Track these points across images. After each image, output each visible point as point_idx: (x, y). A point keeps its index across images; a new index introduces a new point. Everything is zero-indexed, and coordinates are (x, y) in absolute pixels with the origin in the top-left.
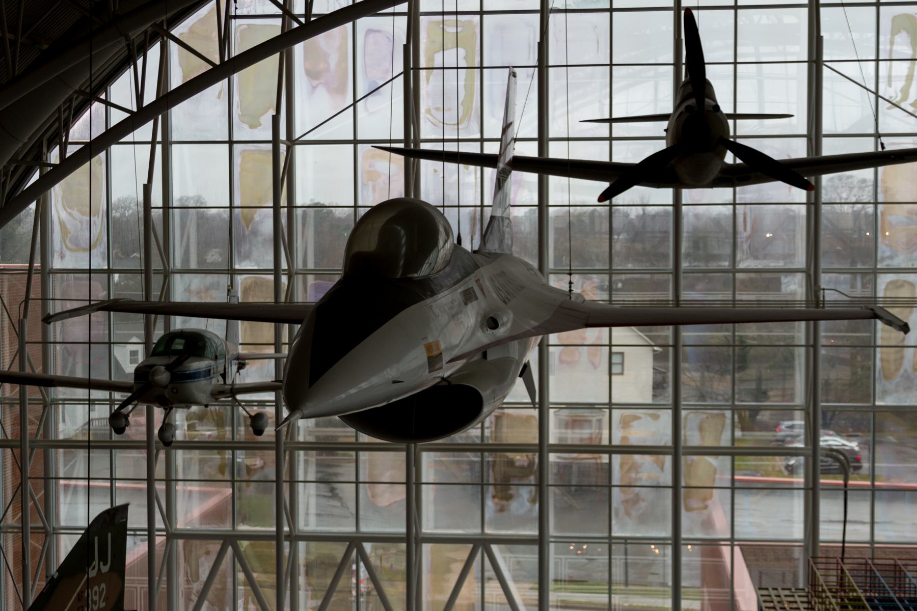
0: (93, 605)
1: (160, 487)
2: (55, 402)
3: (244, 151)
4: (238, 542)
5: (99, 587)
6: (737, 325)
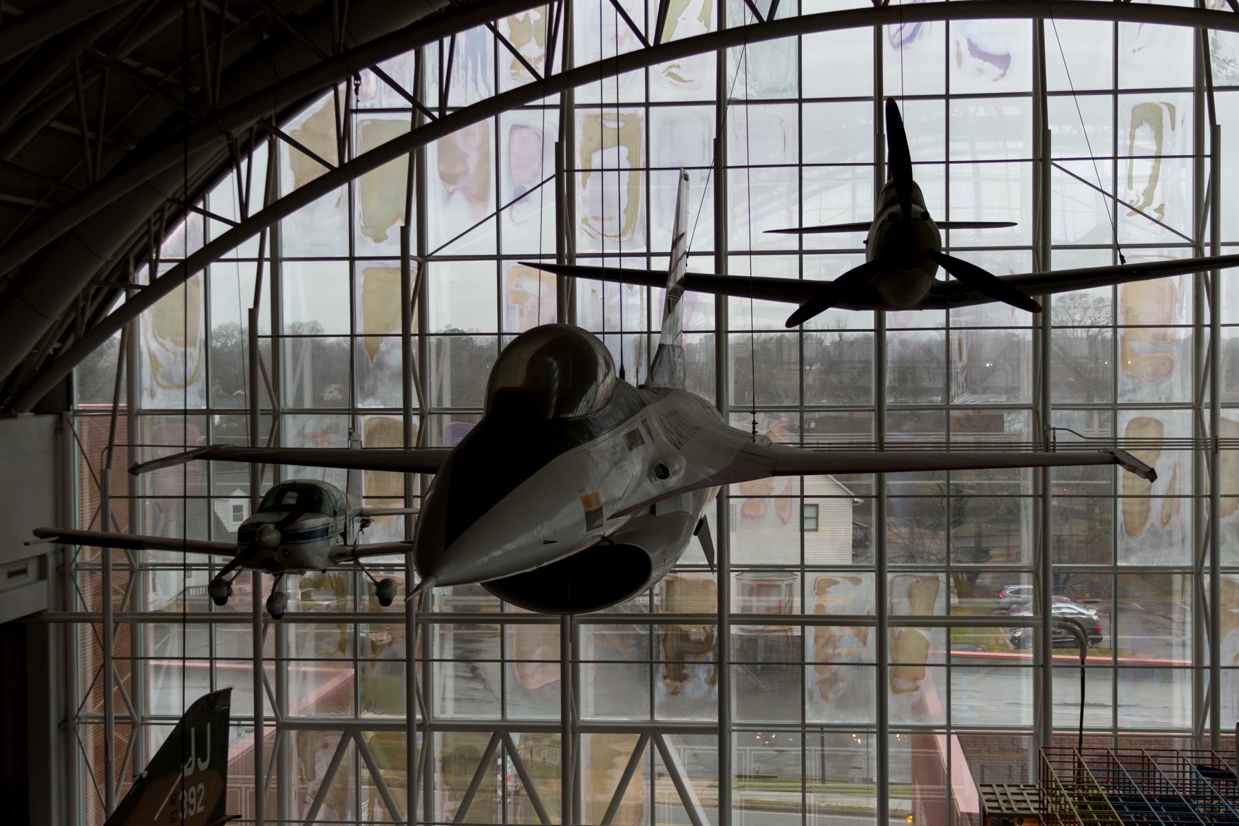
1: (269, 668)
2: (145, 568)
3: (367, 269)
4: (362, 732)
6: (951, 472)
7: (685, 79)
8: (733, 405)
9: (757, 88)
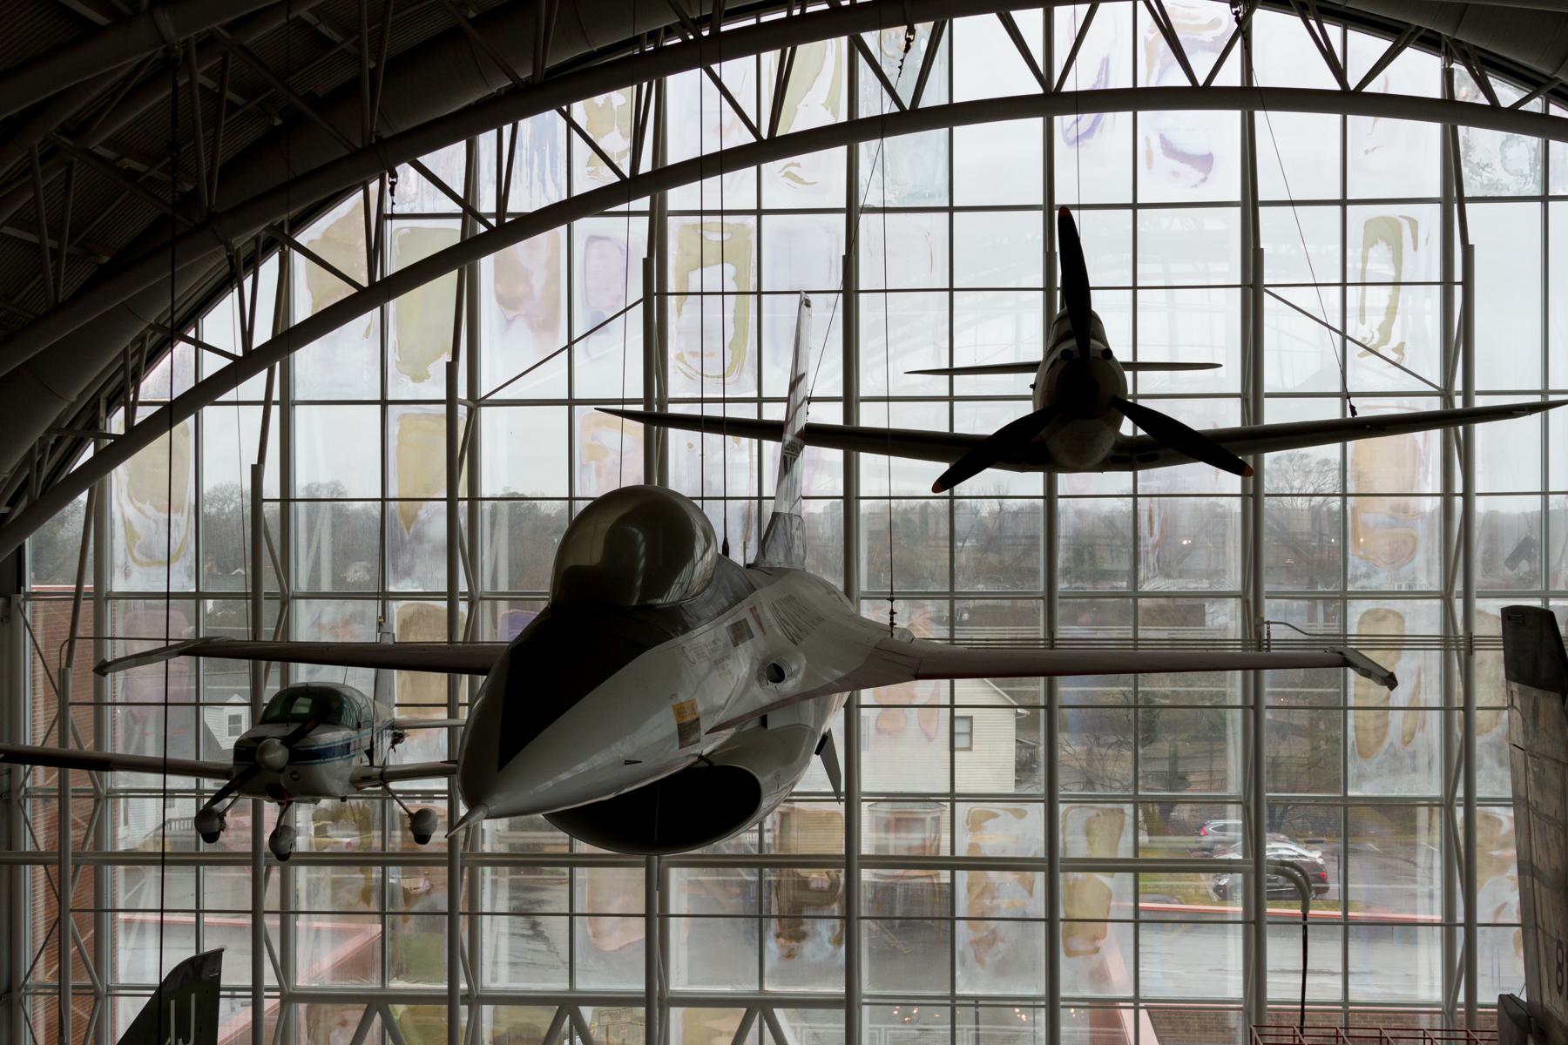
1: (272, 923)
2: (114, 795)
7: (806, 180)
9: (897, 192)
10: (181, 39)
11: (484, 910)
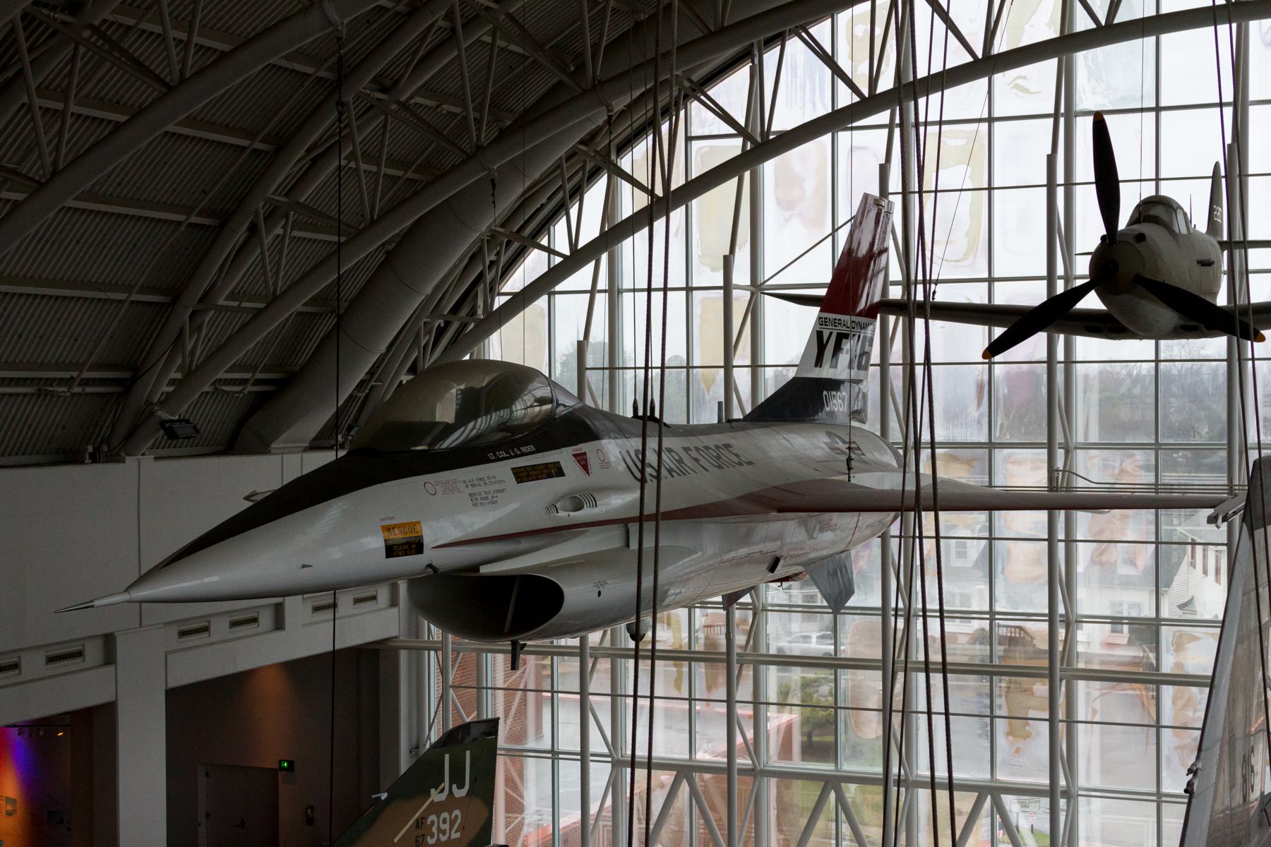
0: (441, 835)
1: (744, 711)
5: (450, 815)
6: (1162, 512)
7: (1031, 90)
8: (1082, 441)
10: (346, 22)
11: (1079, 719)
